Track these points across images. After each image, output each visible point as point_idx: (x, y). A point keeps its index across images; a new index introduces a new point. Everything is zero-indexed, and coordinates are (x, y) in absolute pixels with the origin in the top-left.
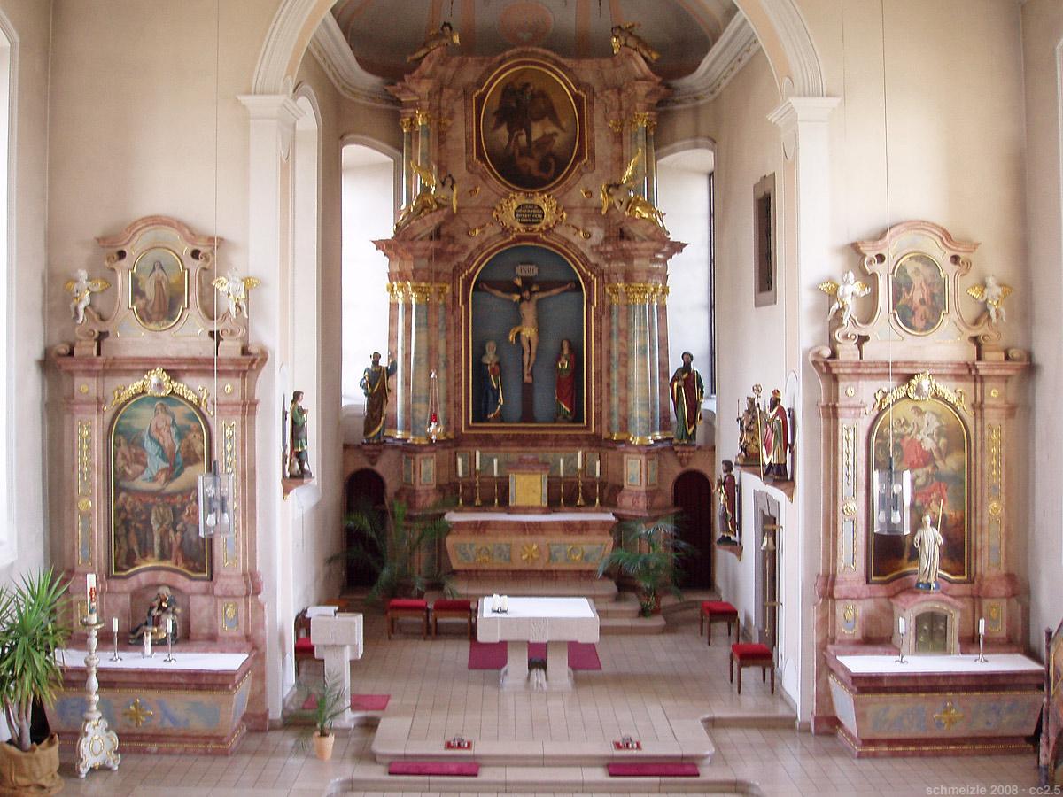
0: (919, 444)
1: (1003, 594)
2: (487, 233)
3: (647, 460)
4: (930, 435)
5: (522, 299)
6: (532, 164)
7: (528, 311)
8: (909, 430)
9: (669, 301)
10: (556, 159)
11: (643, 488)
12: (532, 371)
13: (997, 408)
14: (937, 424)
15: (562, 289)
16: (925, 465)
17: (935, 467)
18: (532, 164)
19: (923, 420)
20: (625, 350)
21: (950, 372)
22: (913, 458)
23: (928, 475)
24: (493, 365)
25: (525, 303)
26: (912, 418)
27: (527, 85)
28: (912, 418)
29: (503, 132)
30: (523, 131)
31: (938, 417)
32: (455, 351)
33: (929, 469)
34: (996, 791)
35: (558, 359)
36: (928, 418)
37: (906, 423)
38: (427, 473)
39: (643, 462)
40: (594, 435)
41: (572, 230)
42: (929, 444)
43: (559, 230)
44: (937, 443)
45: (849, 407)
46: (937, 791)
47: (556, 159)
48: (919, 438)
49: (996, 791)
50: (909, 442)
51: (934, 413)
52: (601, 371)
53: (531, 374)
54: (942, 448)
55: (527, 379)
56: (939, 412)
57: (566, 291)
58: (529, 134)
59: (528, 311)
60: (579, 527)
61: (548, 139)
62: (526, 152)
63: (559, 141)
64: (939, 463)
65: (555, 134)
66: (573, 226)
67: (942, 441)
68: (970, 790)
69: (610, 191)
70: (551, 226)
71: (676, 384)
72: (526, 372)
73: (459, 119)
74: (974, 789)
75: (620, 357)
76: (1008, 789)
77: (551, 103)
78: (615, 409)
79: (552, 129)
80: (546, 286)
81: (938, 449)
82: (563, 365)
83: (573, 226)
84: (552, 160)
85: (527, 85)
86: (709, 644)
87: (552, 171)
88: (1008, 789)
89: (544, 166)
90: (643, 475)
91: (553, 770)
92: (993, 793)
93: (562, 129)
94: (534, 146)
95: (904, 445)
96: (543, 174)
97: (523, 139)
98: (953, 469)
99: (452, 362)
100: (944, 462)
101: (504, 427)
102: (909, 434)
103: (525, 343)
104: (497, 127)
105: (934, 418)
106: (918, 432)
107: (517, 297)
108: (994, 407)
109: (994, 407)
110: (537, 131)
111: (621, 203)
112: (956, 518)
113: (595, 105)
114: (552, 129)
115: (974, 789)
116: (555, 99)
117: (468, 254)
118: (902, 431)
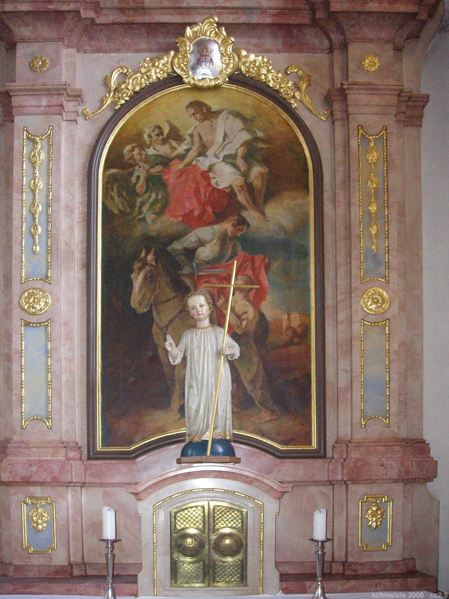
0: (205, 175)
1: (394, 473)
4: (230, 159)
8: (181, 149)
13: (378, 114)
14: (246, 136)
16: (219, 218)
17: (243, 222)
19: (213, 129)
21: (269, 20)
22: (191, 205)
23: (224, 238)
26: (189, 124)
28: (189, 124)
31: (247, 122)
33: (227, 226)
34: (411, 596)
36: (222, 124)
37: (175, 135)
42: (226, 177)
44: (245, 175)
45: (34, 92)
46: (378, 596)
48: (204, 164)
49: (411, 596)
50: (182, 172)
51: (237, 115)
54: (257, 183)
56: (249, 112)
64: (251, 215)
67: (257, 170)
68: (397, 595)
74: (399, 594)
76: (418, 594)
81: (249, 187)
86: (120, 540)
88: (418, 594)
92: (409, 597)
95: (171, 178)
98: (282, 227)
100: (263, 213)
101: (257, 443)
102: (182, 157)
105: (239, 124)
106: (202, 152)
108: (370, 88)
109: (370, 88)
112: (289, 327)
115: (399, 594)
118: (164, 150)
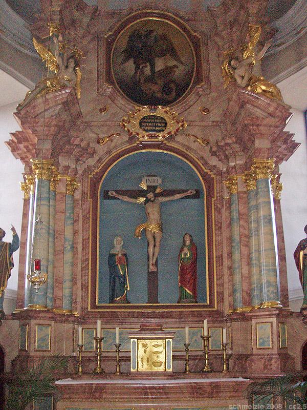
2: (115, 141)
3: (279, 322)
5: (147, 201)
6: (155, 89)
7: (153, 212)
9: (283, 196)
10: (177, 85)
11: (275, 351)
12: (156, 262)
15: (183, 195)
18: (155, 89)
20: (246, 232)
24: (120, 255)
25: (150, 204)
27: (151, 32)
29: (130, 65)
30: (148, 64)
32: (83, 240)
35: (182, 250)
38: (43, 339)
39: (275, 325)
40: (217, 311)
41: (192, 138)
43: (179, 138)
47: (177, 85)
52: (222, 256)
53: (156, 264)
55: (152, 268)
57: (186, 197)
58: (153, 67)
59: (153, 212)
60: (209, 389)
61: (169, 70)
62: (150, 80)
63: (179, 72)
65: (176, 66)
66: (193, 135)
69: (233, 62)
70: (173, 133)
71: (302, 253)
72: (151, 262)
73: (92, 56)
75: (240, 238)
77: (172, 44)
78: (238, 286)
79: (172, 63)
80: (167, 193)
82: (186, 254)
83: (193, 135)
84: (172, 85)
85: (151, 32)
87: (174, 94)
89: (166, 89)
90: (275, 337)
91: (162, 381)
93: (182, 63)
94: (156, 75)
96: (166, 97)
97: (147, 70)
99: (80, 249)
103: (150, 237)
104: (125, 61)
107: (142, 199)
110: (160, 65)
111: (243, 77)
113: (209, 45)
114: (172, 63)
116: (176, 42)
117: (97, 157)
